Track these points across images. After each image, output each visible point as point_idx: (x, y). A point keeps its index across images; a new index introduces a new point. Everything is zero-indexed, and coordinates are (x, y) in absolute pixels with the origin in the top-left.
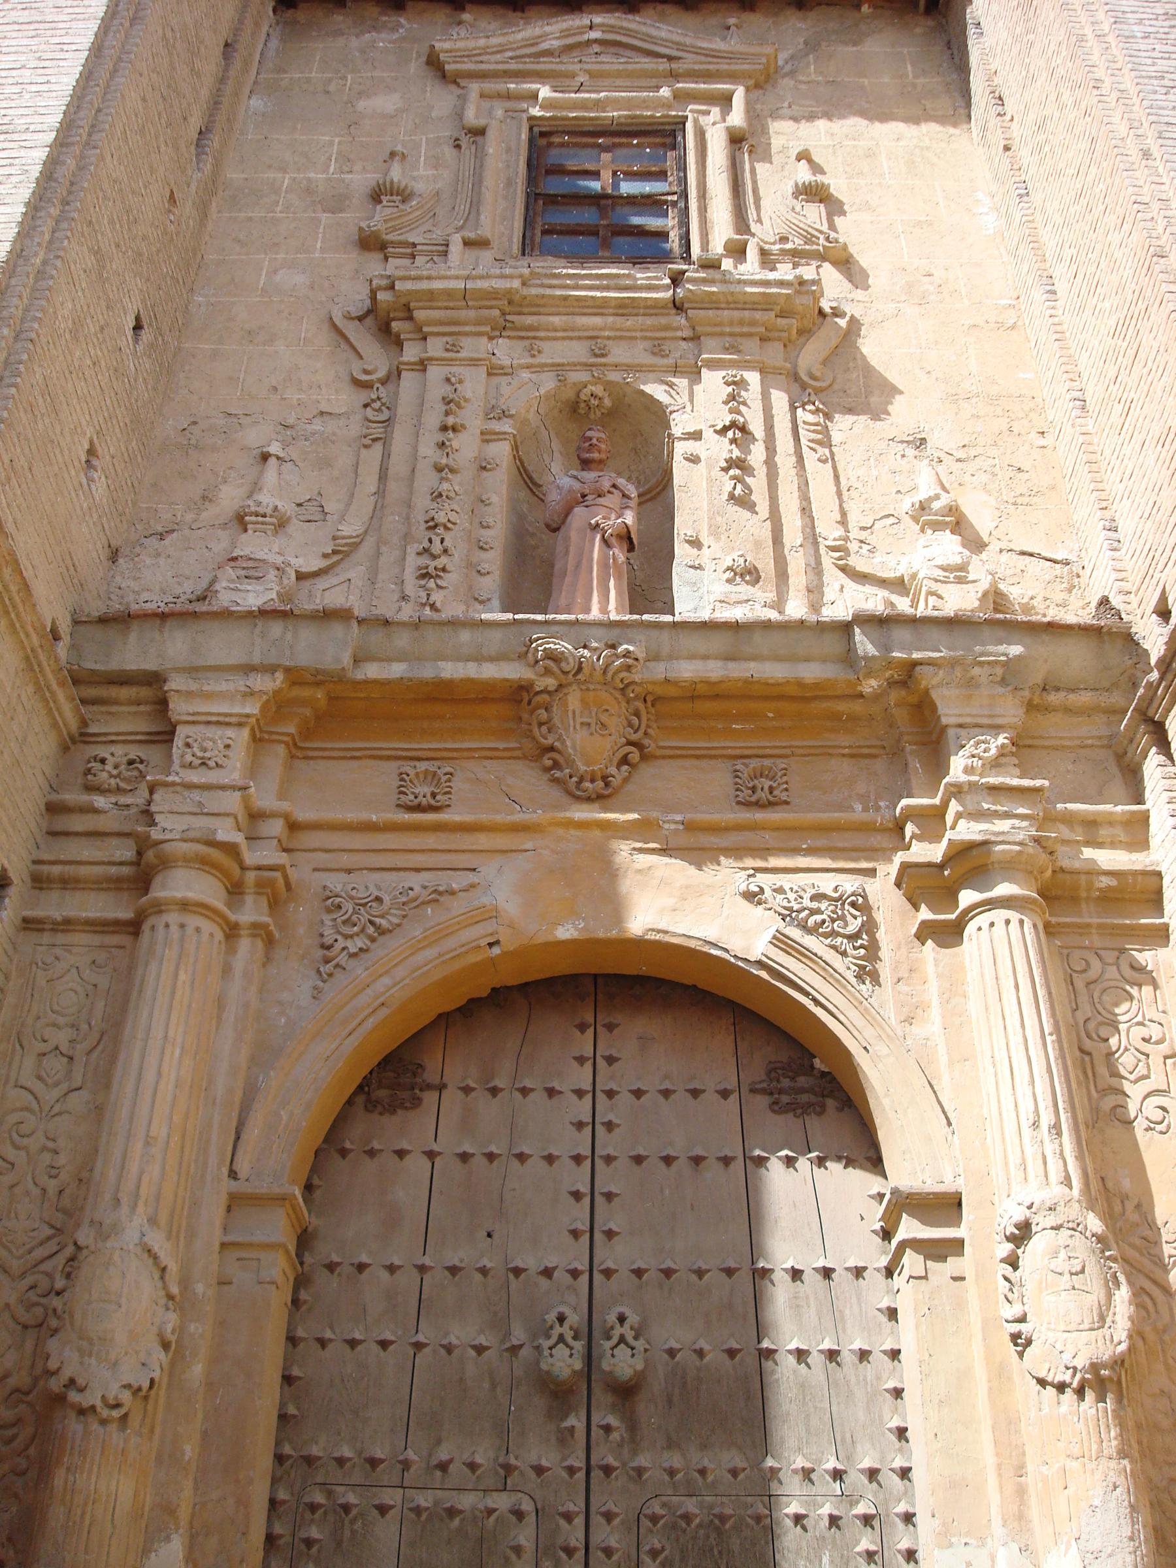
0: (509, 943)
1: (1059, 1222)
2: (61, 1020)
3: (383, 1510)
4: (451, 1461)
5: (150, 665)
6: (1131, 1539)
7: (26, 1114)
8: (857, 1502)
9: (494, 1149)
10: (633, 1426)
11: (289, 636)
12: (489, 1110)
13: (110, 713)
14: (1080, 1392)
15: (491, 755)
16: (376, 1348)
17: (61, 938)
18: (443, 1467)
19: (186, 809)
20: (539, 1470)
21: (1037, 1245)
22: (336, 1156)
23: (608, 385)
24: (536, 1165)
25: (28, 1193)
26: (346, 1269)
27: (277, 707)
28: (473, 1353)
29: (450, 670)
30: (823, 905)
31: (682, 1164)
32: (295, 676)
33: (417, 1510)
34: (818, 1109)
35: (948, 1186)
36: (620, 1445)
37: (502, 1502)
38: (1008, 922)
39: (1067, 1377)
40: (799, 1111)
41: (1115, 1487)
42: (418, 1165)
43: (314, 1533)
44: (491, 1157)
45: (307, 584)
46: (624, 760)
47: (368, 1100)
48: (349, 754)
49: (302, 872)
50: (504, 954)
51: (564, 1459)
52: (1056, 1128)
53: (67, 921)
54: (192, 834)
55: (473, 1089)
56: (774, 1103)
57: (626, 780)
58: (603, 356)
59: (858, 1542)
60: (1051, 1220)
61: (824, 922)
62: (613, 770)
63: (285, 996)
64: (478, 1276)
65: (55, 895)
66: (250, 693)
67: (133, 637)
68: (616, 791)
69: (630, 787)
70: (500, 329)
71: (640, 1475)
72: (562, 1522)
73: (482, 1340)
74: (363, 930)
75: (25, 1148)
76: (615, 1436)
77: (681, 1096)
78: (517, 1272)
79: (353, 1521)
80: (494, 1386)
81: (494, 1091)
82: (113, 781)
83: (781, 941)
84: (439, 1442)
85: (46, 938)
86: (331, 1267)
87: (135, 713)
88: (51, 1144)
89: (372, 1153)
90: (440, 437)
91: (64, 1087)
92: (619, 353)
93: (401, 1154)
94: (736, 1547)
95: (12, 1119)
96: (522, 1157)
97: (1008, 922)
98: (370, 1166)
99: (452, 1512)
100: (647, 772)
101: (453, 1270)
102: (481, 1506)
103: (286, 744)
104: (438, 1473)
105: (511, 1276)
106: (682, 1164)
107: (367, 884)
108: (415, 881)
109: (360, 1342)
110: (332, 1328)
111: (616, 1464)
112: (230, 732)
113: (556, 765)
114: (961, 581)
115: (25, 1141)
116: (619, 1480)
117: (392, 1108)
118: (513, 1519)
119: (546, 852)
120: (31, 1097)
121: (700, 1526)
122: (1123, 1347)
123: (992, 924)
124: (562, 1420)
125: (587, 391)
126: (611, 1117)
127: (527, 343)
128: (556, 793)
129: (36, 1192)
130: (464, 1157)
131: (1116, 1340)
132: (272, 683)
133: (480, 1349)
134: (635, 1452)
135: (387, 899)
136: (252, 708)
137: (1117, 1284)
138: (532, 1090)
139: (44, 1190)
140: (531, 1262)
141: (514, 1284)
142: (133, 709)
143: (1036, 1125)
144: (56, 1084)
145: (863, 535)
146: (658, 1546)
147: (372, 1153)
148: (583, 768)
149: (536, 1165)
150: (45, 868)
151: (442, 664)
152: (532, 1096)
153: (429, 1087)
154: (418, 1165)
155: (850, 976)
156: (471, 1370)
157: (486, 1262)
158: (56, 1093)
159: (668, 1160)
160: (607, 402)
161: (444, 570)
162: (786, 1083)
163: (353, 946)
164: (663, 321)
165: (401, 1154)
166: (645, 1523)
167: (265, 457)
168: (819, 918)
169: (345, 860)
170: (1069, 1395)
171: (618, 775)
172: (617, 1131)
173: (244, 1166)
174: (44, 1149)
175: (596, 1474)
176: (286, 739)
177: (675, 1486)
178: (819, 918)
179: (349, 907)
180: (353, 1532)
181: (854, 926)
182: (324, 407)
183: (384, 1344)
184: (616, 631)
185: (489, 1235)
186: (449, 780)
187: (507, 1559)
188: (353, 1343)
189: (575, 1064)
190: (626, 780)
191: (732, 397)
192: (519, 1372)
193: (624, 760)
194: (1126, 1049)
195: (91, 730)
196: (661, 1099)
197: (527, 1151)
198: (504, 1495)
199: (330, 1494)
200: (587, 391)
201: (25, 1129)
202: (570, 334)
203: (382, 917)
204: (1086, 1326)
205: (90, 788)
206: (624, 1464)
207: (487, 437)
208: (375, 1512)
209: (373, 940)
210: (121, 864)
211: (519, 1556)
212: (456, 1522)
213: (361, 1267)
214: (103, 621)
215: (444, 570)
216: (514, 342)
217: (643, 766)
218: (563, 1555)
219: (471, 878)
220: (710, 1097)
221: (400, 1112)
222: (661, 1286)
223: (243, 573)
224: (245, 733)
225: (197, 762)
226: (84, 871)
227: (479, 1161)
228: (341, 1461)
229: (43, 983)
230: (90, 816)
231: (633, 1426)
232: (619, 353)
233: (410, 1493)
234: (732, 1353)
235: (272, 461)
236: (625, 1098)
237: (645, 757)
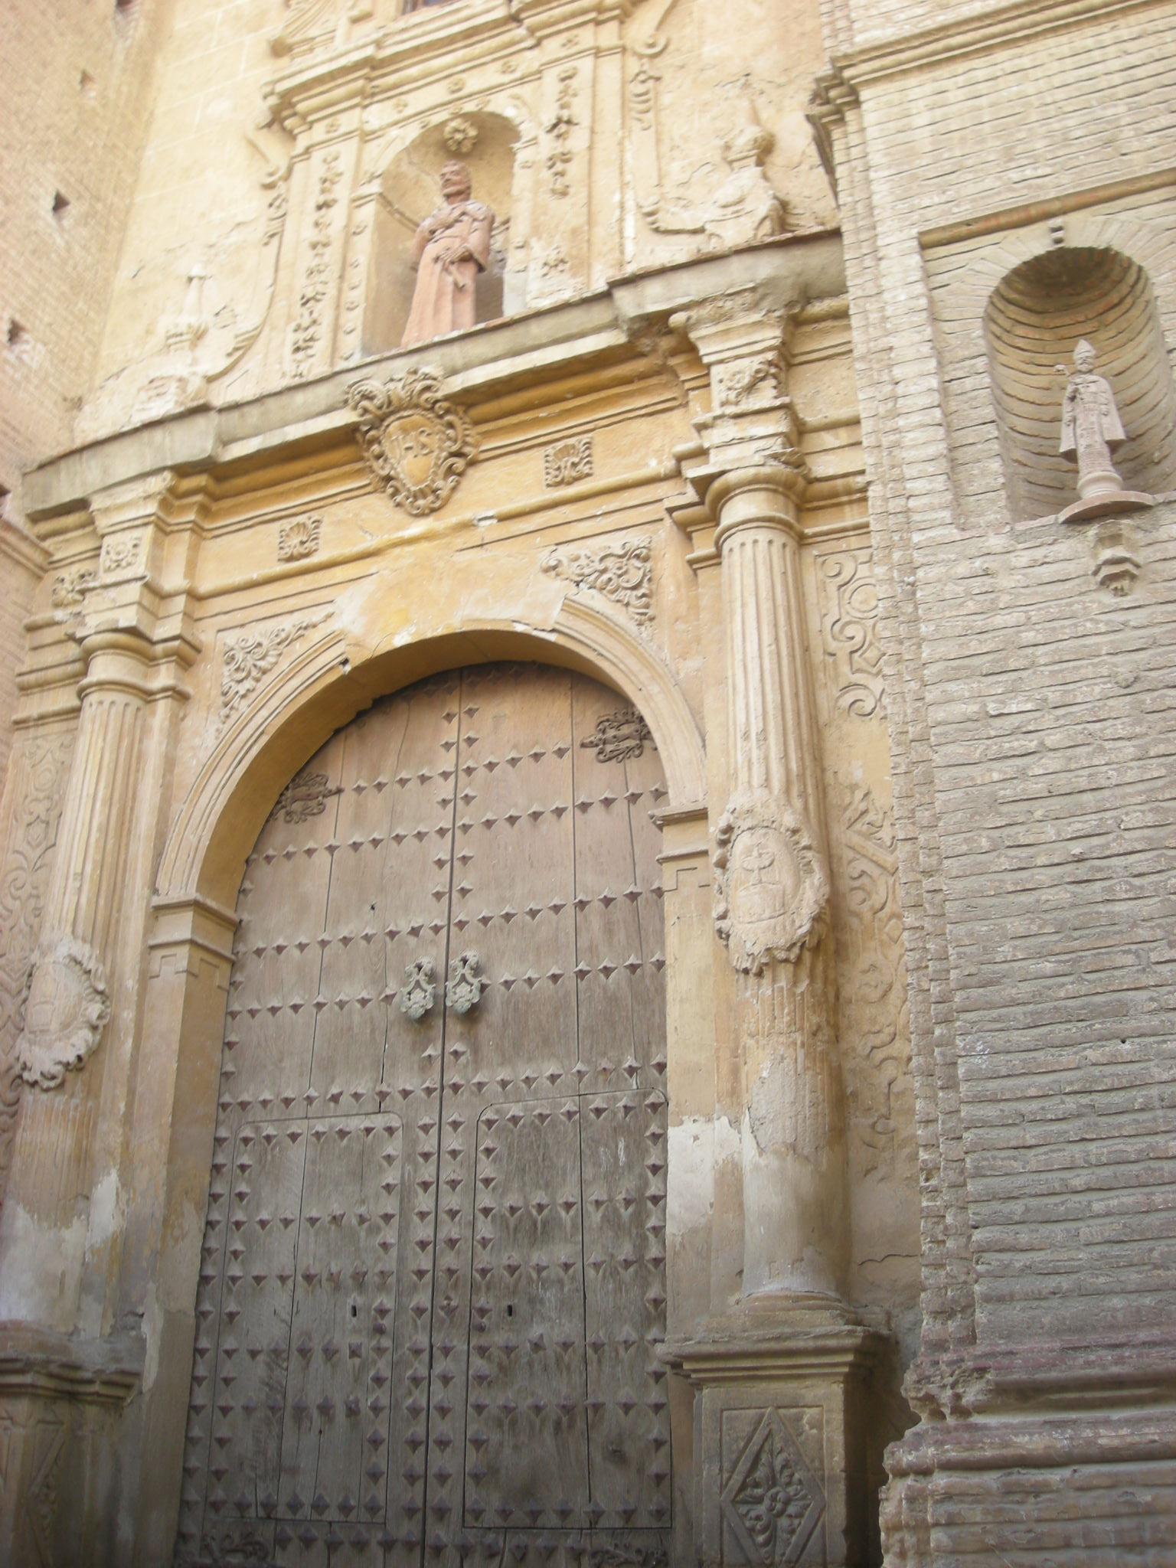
0: (357, 659)
1: (755, 823)
2: (41, 795)
3: (294, 1137)
4: (341, 1094)
5: (78, 495)
6: (793, 1103)
7: (20, 872)
8: (650, 1094)
9: (376, 835)
10: (476, 1050)
11: (167, 440)
12: (376, 803)
13: (67, 541)
14: (760, 974)
15: (349, 496)
16: (290, 1012)
17: (41, 731)
18: (335, 1099)
19: (105, 607)
20: (406, 1094)
21: (742, 842)
22: (263, 863)
23: (466, 116)
24: (410, 843)
25: (21, 931)
26: (271, 952)
27: (171, 499)
28: (358, 1006)
29: (295, 432)
30: (610, 563)
31: (524, 822)
32: (183, 470)
33: (318, 1135)
34: (637, 752)
35: (699, 806)
36: (466, 1066)
37: (378, 1122)
38: (755, 542)
39: (747, 964)
40: (637, 752)
41: (783, 1058)
42: (322, 858)
43: (245, 1160)
44: (375, 842)
45: (215, 385)
46: (450, 471)
47: (288, 814)
48: (249, 523)
49: (205, 634)
50: (355, 669)
51: (424, 1082)
52: (763, 735)
53: (42, 717)
54: (102, 628)
55: (364, 788)
56: (600, 753)
57: (454, 489)
58: (459, 90)
59: (647, 1127)
60: (748, 823)
61: (610, 580)
62: (440, 483)
63: (197, 741)
64: (363, 943)
65: (36, 698)
66: (147, 497)
67: (63, 475)
68: (446, 501)
69: (458, 495)
70: (367, 97)
71: (480, 1090)
72: (421, 1134)
73: (364, 995)
74: (249, 673)
75: (19, 898)
76: (463, 1059)
77: (526, 763)
78: (392, 934)
79: (273, 1149)
80: (373, 1031)
81: (380, 786)
82: (70, 596)
83: (571, 607)
84: (333, 1081)
85: (32, 732)
86: (259, 952)
87: (83, 535)
88: (34, 892)
89: (289, 856)
90: (316, 215)
91: (44, 846)
92: (474, 82)
93: (310, 852)
94: (550, 1142)
95: (10, 878)
96: (399, 839)
97: (770, 542)
98: (288, 866)
99: (342, 1134)
100: (474, 474)
101: (346, 941)
102: (362, 1127)
103: (191, 530)
104: (332, 1104)
105: (388, 939)
106: (524, 822)
107: (256, 633)
108: (288, 624)
109: (279, 1009)
110: (259, 1001)
111: (462, 1082)
112: (137, 533)
113: (396, 492)
114: (737, 215)
115: (19, 893)
116: (464, 1095)
117: (306, 814)
118: (386, 1134)
119: (386, 572)
120: (21, 858)
121: (524, 1126)
122: (805, 929)
123: (743, 545)
124: (424, 1051)
125: (448, 129)
126: (468, 791)
127: (394, 101)
128: (399, 516)
129: (26, 929)
130: (356, 846)
131: (797, 924)
132: (158, 484)
133: (364, 1002)
134: (476, 1070)
135: (265, 643)
136: (152, 508)
137: (811, 872)
138: (408, 780)
139: (31, 927)
140: (404, 927)
141: (390, 944)
142: (80, 532)
143: (746, 736)
144: (38, 845)
145: (680, 192)
146: (491, 1146)
147: (289, 856)
148: (413, 489)
149: (410, 843)
150: (25, 678)
151: (287, 429)
152: (409, 785)
153: (331, 793)
154: (322, 858)
155: (632, 627)
156: (356, 1018)
157: (369, 931)
158: (39, 851)
159: (512, 820)
160: (472, 132)
161: (311, 339)
162: (611, 733)
163: (242, 689)
164: (505, 38)
165: (310, 852)
166: (483, 1127)
167: (190, 279)
168: (605, 577)
169: (239, 617)
170: (752, 979)
171: (444, 485)
172: (473, 802)
173: (162, 883)
174: (31, 896)
175: (448, 1091)
176: (189, 526)
177: (506, 1097)
178: (605, 577)
179: (240, 656)
180: (273, 1157)
181: (634, 577)
182: (239, 219)
183: (296, 1008)
184: (415, 358)
185: (373, 908)
186: (316, 527)
187: (381, 1166)
188: (274, 1010)
189: (443, 750)
190: (454, 489)
191: (564, 92)
192: (392, 1017)
193: (450, 471)
194: (871, 644)
195: (55, 558)
196: (509, 767)
197: (402, 833)
198: (380, 1116)
199: (257, 1130)
200: (448, 129)
201: (19, 884)
202: (428, 79)
203: (263, 658)
204: (767, 915)
205: (58, 605)
206: (468, 1081)
207: (358, 202)
208: (289, 1141)
209: (258, 680)
210: (74, 661)
211: (390, 1164)
212: (345, 1141)
213: (280, 949)
214: (41, 467)
215: (311, 339)
216: (386, 103)
217: (471, 471)
218: (421, 1160)
219: (329, 609)
220: (550, 759)
221: (309, 818)
222: (501, 929)
223: (155, 392)
224: (150, 529)
225: (114, 565)
226: (51, 674)
227: (367, 847)
228: (265, 1103)
229: (29, 769)
230: (55, 628)
231: (476, 1050)
232: (474, 82)
233: (312, 1122)
234: (555, 978)
235: (195, 282)
236: (481, 773)
237: (473, 463)
